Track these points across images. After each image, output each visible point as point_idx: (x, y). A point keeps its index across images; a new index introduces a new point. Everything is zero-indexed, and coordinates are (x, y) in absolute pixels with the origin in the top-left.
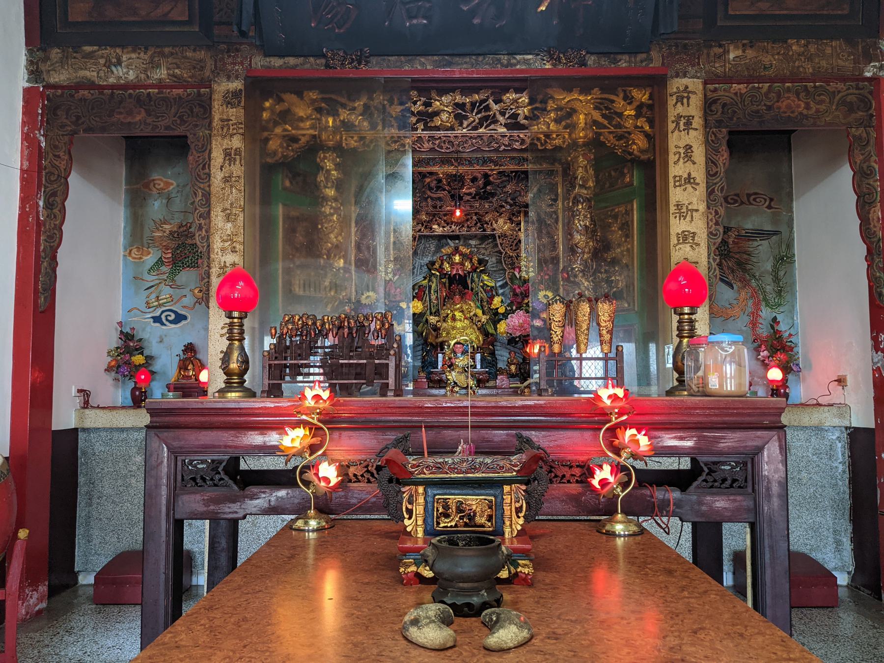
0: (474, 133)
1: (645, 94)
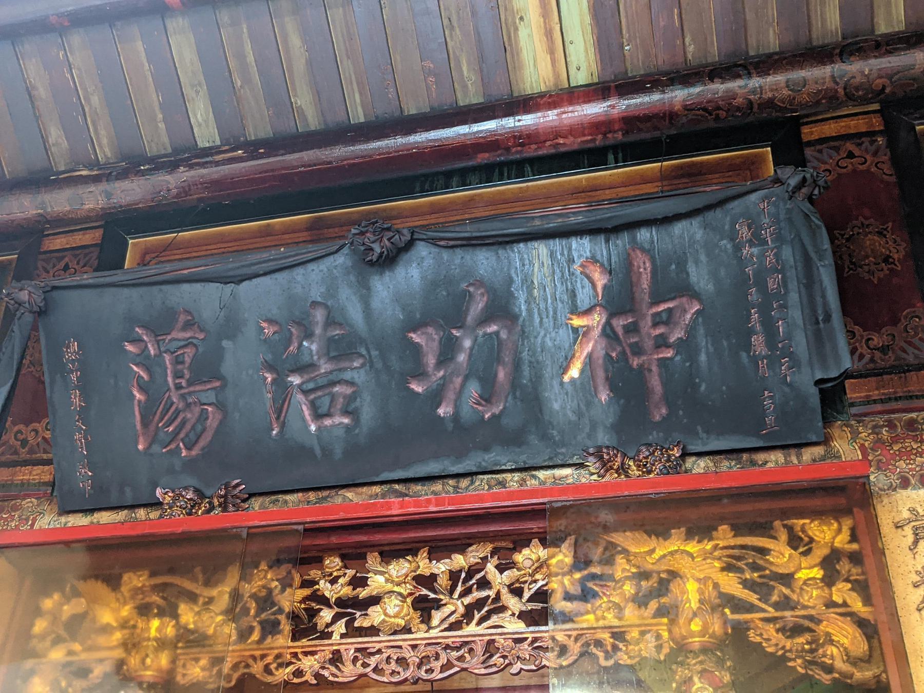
0: (455, 637)
1: (839, 531)
